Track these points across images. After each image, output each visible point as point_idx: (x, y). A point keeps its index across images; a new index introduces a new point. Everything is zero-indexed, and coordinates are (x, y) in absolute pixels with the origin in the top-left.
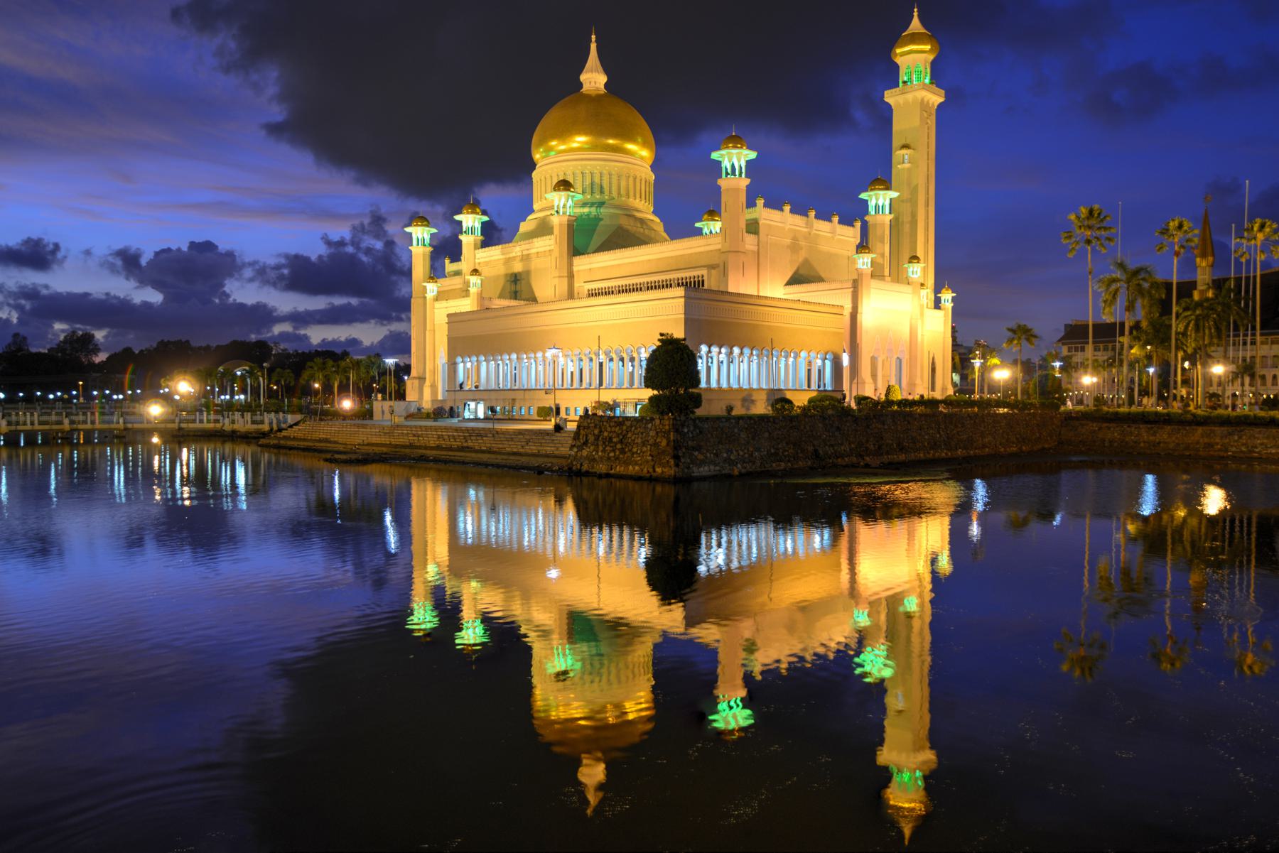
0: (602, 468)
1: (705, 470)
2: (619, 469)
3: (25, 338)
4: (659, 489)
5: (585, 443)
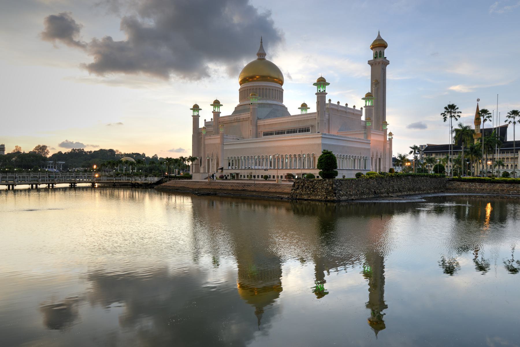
0: (306, 197)
1: (344, 198)
2: (313, 197)
3: (20, 148)
4: (329, 204)
5: (298, 188)
